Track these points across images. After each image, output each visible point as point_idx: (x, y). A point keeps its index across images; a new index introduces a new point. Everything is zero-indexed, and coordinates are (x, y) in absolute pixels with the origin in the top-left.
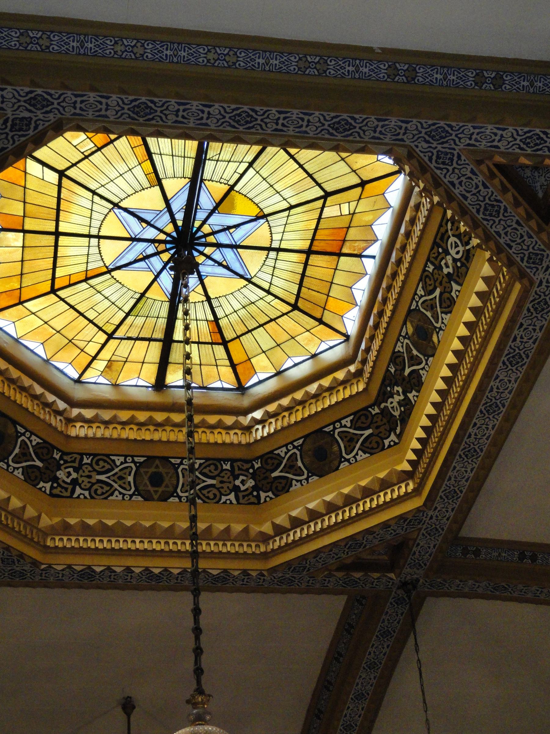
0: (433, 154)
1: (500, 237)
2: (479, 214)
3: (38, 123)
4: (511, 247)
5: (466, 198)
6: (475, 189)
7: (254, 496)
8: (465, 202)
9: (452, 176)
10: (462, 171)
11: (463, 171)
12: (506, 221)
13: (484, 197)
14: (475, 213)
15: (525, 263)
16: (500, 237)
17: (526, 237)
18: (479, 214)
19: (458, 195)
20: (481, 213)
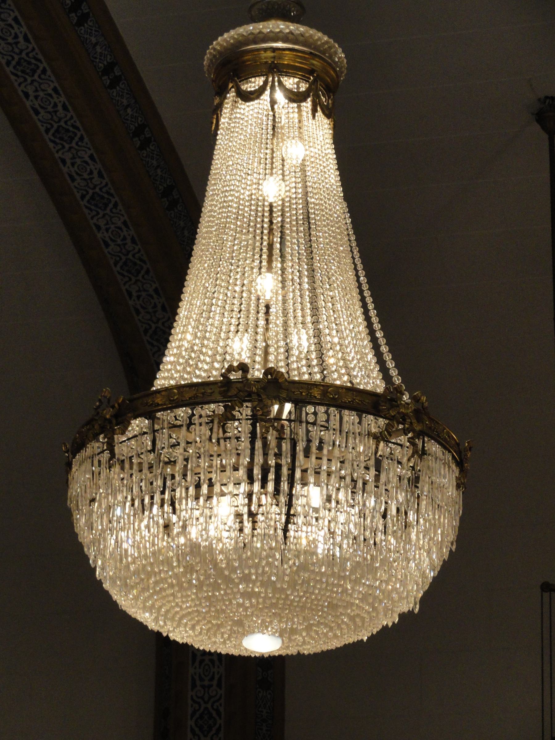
0: (143, 277)
1: (133, 237)
2: (116, 202)
3: (215, 707)
4: (55, 90)
5: (16, 19)
6: (110, 228)
7: (213, 612)
8: (57, 85)
9: (24, 47)
10: (10, 48)
11: (83, 183)
12: (12, 51)
13: (159, 320)
14: (85, 136)
15: (113, 200)
16: (133, 237)
17: (103, 227)
18: (116, 202)
19: (63, 95)
20: (41, 68)
